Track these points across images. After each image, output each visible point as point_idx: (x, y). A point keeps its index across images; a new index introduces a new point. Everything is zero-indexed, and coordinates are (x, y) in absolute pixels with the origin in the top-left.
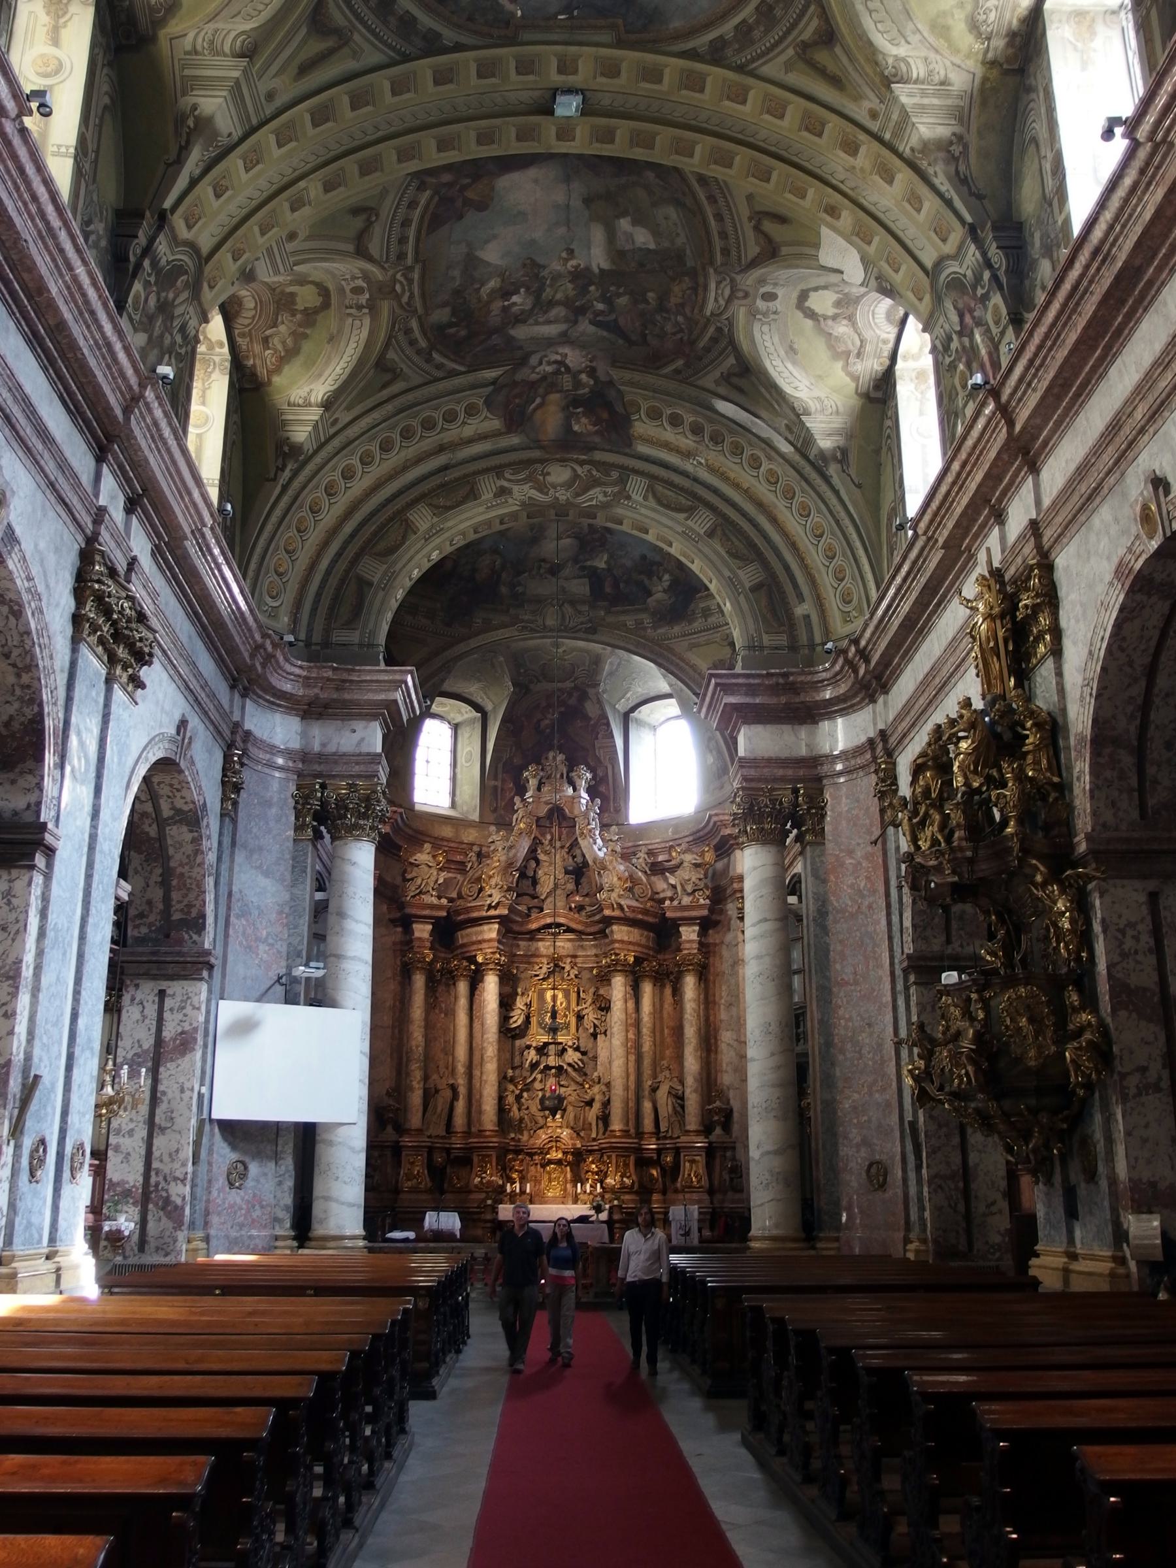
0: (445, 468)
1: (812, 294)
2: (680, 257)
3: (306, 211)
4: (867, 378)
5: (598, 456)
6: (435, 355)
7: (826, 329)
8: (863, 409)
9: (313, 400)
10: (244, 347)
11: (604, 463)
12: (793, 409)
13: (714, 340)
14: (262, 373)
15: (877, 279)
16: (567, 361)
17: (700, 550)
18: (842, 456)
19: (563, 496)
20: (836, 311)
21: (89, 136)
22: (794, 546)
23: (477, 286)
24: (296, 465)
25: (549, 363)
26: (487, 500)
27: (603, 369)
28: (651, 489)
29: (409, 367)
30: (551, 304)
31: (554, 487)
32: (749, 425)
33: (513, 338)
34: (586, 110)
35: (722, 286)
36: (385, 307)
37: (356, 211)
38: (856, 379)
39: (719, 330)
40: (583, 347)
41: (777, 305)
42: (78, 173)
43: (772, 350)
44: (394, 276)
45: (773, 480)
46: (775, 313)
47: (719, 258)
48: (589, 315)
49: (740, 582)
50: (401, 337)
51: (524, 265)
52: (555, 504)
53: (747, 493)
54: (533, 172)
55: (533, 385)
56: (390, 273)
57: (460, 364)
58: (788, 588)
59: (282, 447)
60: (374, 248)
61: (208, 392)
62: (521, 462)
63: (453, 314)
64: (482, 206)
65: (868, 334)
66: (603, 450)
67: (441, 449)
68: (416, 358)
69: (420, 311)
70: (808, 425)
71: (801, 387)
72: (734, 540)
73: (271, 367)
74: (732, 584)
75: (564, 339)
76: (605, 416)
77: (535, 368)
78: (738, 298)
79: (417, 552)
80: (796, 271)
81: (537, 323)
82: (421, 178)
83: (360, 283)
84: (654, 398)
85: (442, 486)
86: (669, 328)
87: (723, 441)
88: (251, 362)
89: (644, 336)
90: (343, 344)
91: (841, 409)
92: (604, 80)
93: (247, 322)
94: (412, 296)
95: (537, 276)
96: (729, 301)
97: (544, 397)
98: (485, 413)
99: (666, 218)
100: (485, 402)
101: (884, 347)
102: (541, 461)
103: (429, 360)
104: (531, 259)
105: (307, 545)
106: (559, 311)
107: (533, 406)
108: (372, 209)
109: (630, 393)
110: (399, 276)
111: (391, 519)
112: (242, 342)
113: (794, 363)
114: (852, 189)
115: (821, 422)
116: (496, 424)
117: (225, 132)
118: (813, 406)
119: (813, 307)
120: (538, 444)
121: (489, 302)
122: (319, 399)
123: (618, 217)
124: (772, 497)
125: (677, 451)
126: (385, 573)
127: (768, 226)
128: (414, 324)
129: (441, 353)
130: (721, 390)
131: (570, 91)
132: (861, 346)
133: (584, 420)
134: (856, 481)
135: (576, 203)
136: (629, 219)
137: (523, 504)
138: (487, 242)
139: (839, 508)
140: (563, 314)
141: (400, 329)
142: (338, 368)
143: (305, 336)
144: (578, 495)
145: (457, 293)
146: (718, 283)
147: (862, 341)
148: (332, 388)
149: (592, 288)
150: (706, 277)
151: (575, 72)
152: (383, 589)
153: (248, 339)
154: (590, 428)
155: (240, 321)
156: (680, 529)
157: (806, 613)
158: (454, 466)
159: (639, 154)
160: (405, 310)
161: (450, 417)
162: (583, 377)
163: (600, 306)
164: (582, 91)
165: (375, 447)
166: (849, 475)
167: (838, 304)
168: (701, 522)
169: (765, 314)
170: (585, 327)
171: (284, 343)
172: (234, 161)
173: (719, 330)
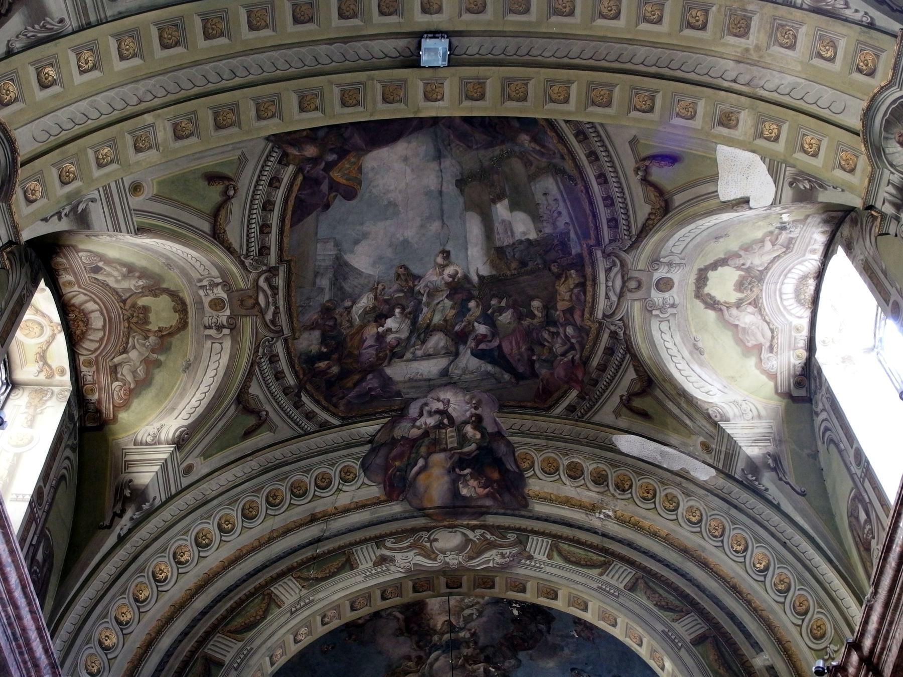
0: (318, 540)
1: (711, 274)
2: (564, 244)
3: (151, 156)
4: (786, 374)
5: (491, 520)
6: (305, 398)
7: (731, 320)
8: (788, 411)
9: (163, 437)
10: (89, 378)
11: (499, 527)
12: (708, 417)
13: (610, 351)
14: (107, 408)
15: (791, 184)
16: (450, 410)
17: (622, 605)
18: (775, 463)
19: (453, 560)
20: (740, 295)
21: (46, 491)
22: (735, 590)
23: (348, 303)
24: (137, 515)
25: (431, 414)
26: (366, 570)
27: (488, 414)
28: (555, 548)
29: (275, 410)
30: (430, 330)
31: (443, 552)
32: (658, 460)
33: (390, 379)
34: (454, 60)
35: (612, 275)
36: (248, 325)
37: (212, 178)
38: (773, 376)
39: (614, 335)
40: (466, 389)
41: (673, 295)
42: (30, 518)
43: (674, 351)
44: (256, 281)
45: (694, 519)
46: (673, 306)
47: (606, 234)
48: (471, 343)
49: (679, 636)
50: (265, 365)
51: (398, 276)
52: (445, 571)
53: (667, 540)
54: (401, 148)
55: (414, 443)
56: (252, 276)
57: (334, 414)
58: (738, 638)
59: (122, 490)
60: (233, 233)
61: (39, 417)
62: (404, 531)
63: (324, 340)
64: (350, 194)
65: (777, 323)
66: (496, 514)
67: (313, 519)
68: (283, 399)
69: (287, 332)
70: (729, 431)
71: (714, 390)
72: (661, 592)
73: (118, 401)
74: (669, 639)
75: (446, 379)
76: (496, 475)
77: (415, 420)
78: (630, 291)
79: (281, 626)
80: (692, 226)
81: (415, 359)
82: (279, 140)
83: (220, 293)
84: (547, 447)
85: (314, 558)
86: (559, 348)
87: (631, 487)
88: (96, 396)
89: (532, 363)
90: (200, 373)
91: (763, 413)
92: (467, 17)
93: (93, 346)
94: (276, 313)
95: (412, 289)
96: (621, 296)
97: (426, 459)
98: (362, 478)
99: (545, 194)
100: (363, 465)
101: (798, 335)
102: (427, 529)
103: (298, 405)
104: (404, 266)
105: (146, 618)
106: (437, 340)
107: (416, 469)
108: (229, 179)
109: (523, 446)
110: (262, 282)
111: (251, 594)
112: (87, 372)
113: (701, 364)
114: (748, 84)
115: (743, 428)
116: (374, 491)
117: (57, 15)
118: (730, 411)
119: (714, 293)
120: (422, 511)
121: (362, 327)
122: (170, 436)
123: (494, 202)
124: (697, 539)
125: (581, 506)
126: (241, 650)
127: (660, 174)
128: (279, 348)
129: (311, 396)
130: (622, 423)
131: (435, 34)
132: (773, 337)
133: (473, 483)
134: (798, 489)
135: (450, 188)
136: (506, 202)
137: (408, 570)
138: (357, 242)
139: (784, 525)
140: (442, 344)
141: (264, 354)
142: (194, 400)
143: (158, 364)
144: (471, 558)
145: (327, 311)
146: (608, 271)
147: (772, 331)
148: (186, 423)
149: (472, 304)
150: (593, 264)
151: (439, 10)
152: (236, 669)
153: (94, 368)
154: (480, 491)
155: (87, 345)
156: (595, 585)
157: (767, 663)
158: (327, 538)
159: (512, 109)
160: (271, 330)
161: (324, 483)
162: (469, 429)
163: (482, 329)
164: (448, 34)
165: (235, 514)
166: (787, 483)
167: (740, 286)
168: (619, 577)
169: (662, 309)
170: (468, 361)
171: (134, 373)
172: (63, 49)
173: (614, 335)
